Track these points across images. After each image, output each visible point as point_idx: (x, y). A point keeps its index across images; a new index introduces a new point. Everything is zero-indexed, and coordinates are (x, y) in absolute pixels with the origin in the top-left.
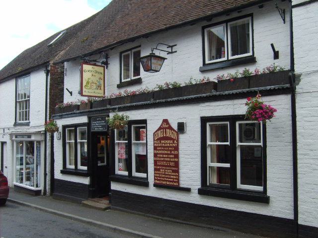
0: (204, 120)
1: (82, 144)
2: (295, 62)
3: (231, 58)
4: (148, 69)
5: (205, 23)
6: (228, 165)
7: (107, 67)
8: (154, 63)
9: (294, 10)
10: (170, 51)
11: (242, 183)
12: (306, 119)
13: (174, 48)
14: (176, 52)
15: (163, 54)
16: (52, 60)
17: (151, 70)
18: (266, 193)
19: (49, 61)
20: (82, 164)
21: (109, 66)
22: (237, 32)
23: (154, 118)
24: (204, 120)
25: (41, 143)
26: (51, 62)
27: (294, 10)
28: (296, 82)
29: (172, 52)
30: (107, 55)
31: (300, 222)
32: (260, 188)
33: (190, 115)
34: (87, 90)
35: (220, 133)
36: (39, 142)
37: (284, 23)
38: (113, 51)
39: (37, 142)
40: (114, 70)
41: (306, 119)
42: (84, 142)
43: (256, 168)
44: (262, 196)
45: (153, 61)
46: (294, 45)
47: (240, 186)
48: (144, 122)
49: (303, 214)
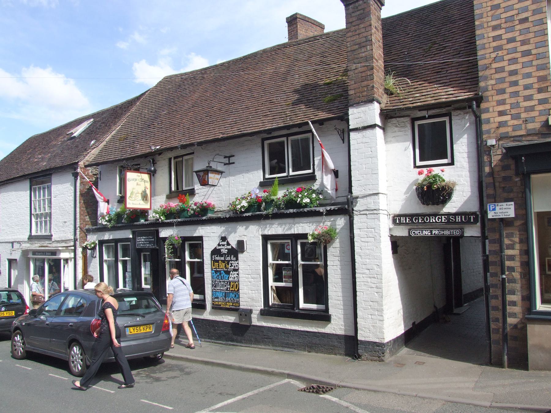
0: (266, 238)
1: (125, 263)
2: (353, 185)
3: (291, 173)
4: (204, 183)
5: (265, 136)
6: (472, 221)
7: (153, 175)
8: (211, 178)
9: (352, 134)
10: (228, 162)
11: (305, 302)
12: (362, 239)
13: (231, 158)
14: (234, 163)
15: (220, 168)
16: (81, 160)
17: (208, 184)
18: (328, 312)
19: (78, 162)
20: (146, 284)
21: (156, 175)
22: (476, 406)
23: (211, 236)
24: (266, 238)
25: (69, 261)
26: (81, 164)
27: (352, 134)
28: (354, 204)
29: (229, 164)
30: (153, 160)
31: (360, 338)
32: (322, 307)
33: (251, 235)
34: (131, 202)
35: (280, 254)
36: (66, 260)
37: (343, 143)
38: (161, 156)
39: (64, 260)
40: (164, 180)
41: (362, 239)
42: (126, 260)
43: (318, 288)
44: (323, 314)
45: (210, 175)
46: (352, 167)
47: (302, 305)
48: (200, 238)
49: (362, 330)
